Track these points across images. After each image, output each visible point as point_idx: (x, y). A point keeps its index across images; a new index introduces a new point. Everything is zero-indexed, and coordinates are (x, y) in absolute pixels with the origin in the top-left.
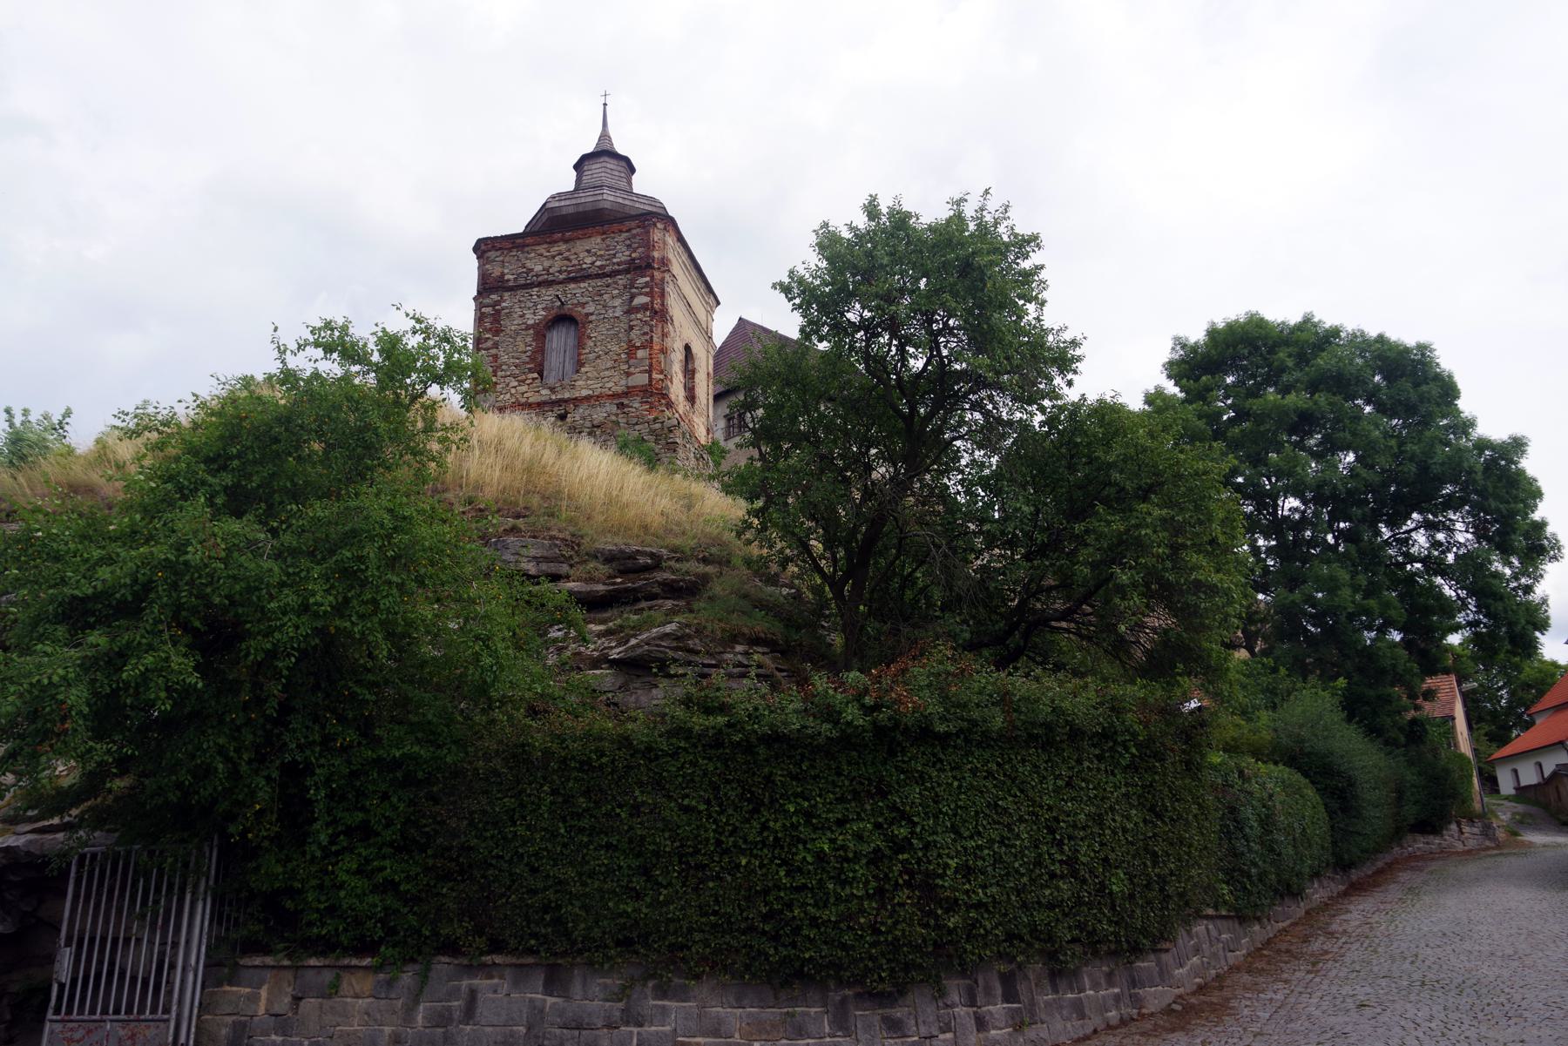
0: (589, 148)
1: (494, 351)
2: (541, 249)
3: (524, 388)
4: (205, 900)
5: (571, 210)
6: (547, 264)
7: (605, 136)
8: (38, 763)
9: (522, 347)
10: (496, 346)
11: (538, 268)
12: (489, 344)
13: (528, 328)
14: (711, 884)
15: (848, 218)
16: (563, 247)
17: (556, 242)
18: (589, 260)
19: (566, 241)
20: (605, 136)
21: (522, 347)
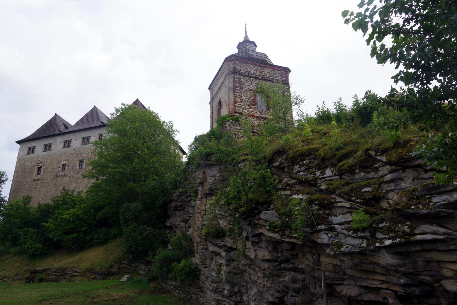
0: (242, 40)
1: (240, 94)
2: (252, 66)
3: (252, 110)
4: (444, 234)
5: (257, 57)
6: (255, 72)
7: (246, 37)
8: (269, 207)
9: (249, 96)
10: (241, 92)
11: (252, 72)
12: (238, 91)
13: (250, 90)
14: (413, 207)
15: (119, 106)
16: (260, 68)
17: (257, 66)
18: (268, 75)
19: (260, 67)
20: (246, 37)
21: (249, 96)
